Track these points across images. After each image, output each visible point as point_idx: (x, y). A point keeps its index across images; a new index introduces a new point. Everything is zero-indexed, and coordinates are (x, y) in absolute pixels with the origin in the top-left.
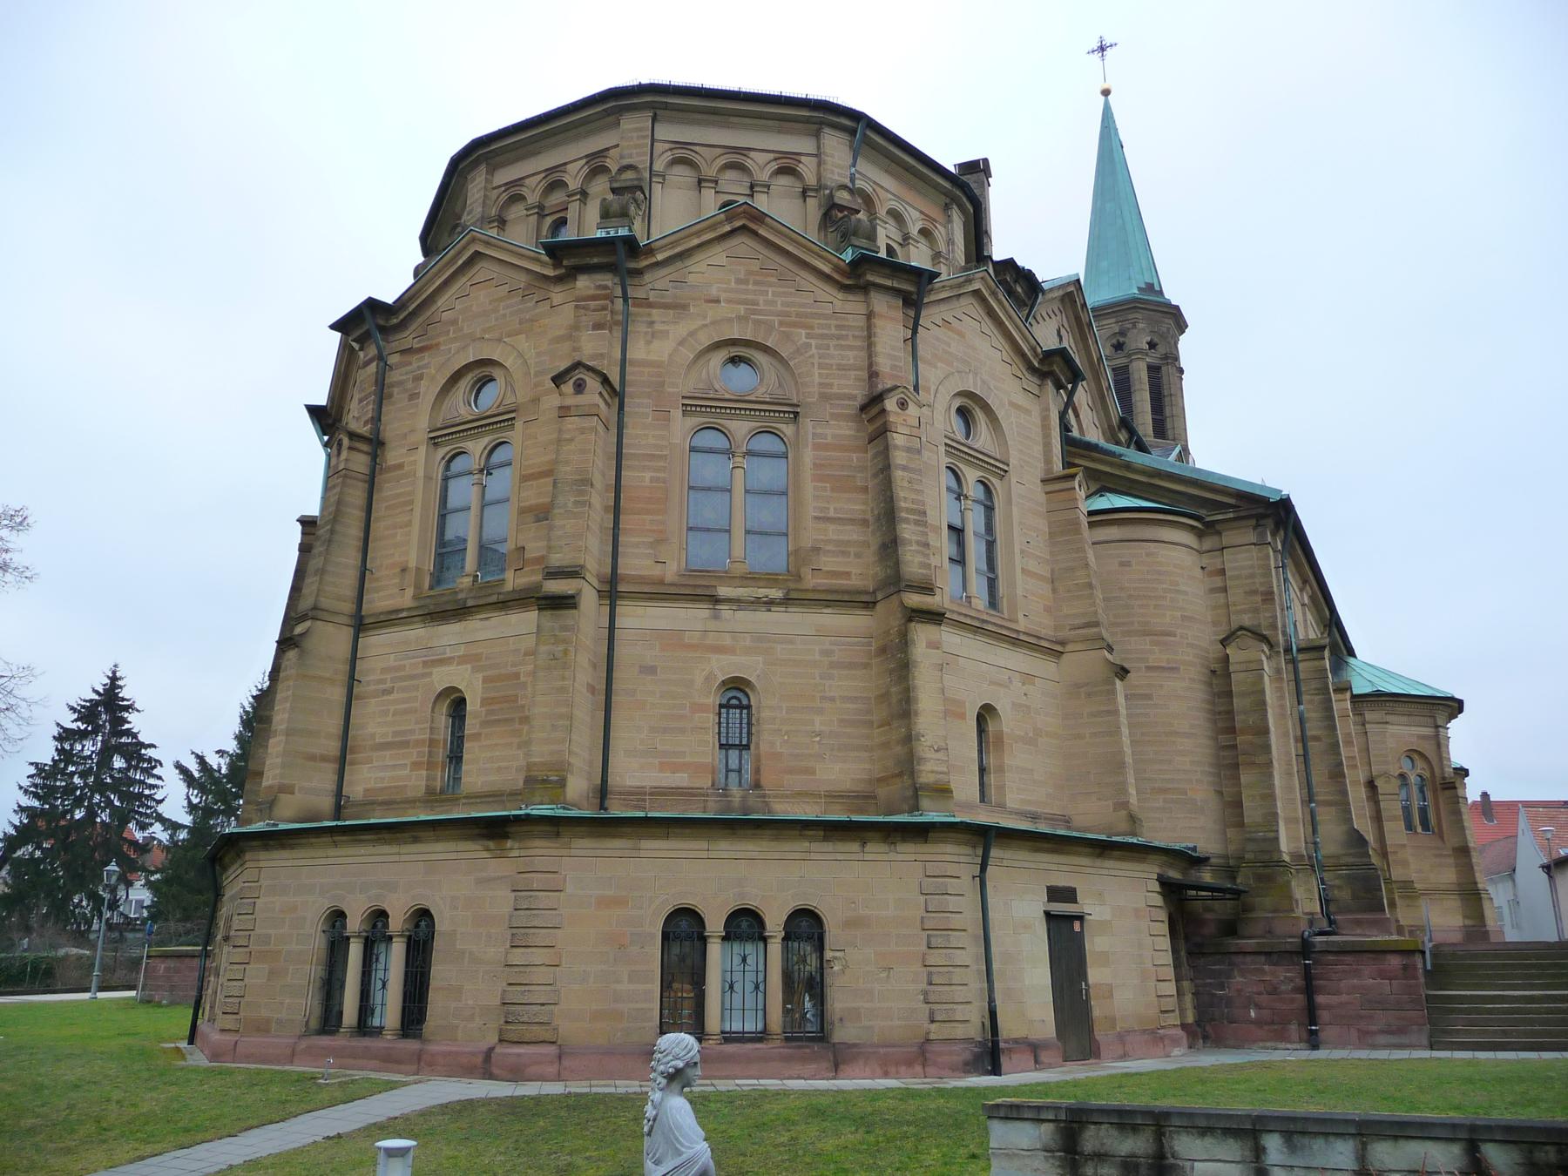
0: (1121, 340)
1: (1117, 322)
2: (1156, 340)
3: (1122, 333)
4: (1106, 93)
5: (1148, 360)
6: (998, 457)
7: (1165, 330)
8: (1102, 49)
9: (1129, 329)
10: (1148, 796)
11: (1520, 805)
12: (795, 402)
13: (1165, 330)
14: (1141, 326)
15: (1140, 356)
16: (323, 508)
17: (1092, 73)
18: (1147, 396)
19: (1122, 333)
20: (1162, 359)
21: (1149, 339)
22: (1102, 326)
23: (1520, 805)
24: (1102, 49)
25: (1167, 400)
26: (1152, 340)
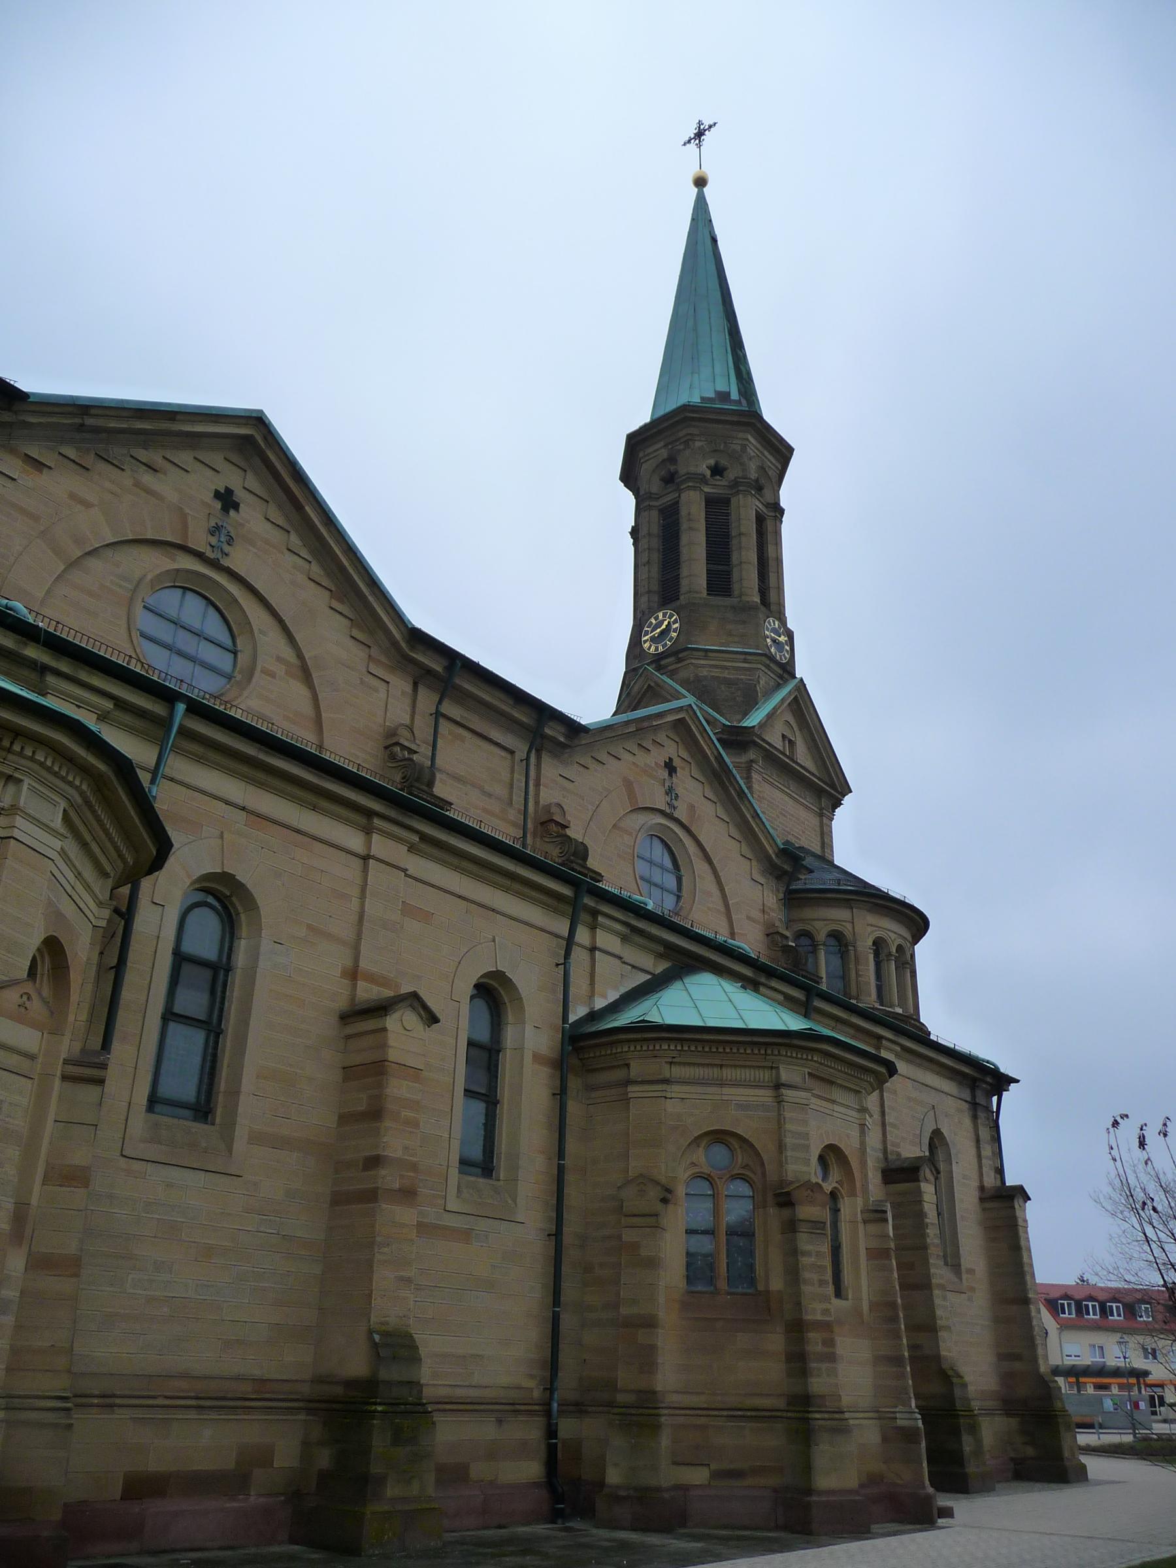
0: (672, 468)
1: (665, 446)
2: (724, 462)
3: (672, 459)
4: (700, 182)
5: (707, 489)
6: (152, 604)
7: (738, 448)
8: (700, 134)
9: (679, 451)
10: (480, 1305)
11: (459, 664)
12: (160, 786)
13: (738, 448)
14: (698, 444)
15: (690, 484)
16: (1007, 1187)
17: (688, 162)
18: (701, 538)
19: (672, 459)
20: (730, 487)
21: (712, 462)
22: (648, 455)
23: (459, 664)
24: (700, 134)
25: (734, 542)
26: (717, 464)
